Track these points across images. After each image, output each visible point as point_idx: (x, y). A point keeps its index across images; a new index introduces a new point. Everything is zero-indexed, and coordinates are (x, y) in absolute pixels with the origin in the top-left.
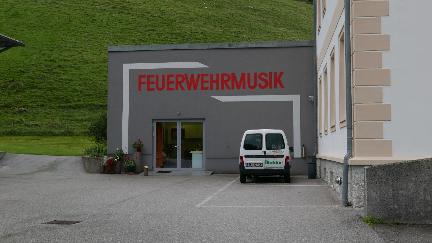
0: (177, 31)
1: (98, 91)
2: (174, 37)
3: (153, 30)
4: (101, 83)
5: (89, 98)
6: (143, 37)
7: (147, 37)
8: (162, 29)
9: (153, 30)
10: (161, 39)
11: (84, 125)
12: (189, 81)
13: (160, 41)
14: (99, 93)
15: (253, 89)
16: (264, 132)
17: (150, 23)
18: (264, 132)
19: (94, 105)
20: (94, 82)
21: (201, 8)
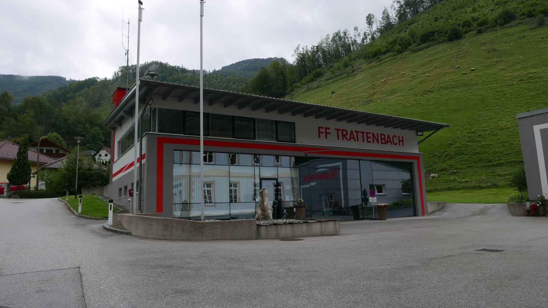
20: (511, 144)
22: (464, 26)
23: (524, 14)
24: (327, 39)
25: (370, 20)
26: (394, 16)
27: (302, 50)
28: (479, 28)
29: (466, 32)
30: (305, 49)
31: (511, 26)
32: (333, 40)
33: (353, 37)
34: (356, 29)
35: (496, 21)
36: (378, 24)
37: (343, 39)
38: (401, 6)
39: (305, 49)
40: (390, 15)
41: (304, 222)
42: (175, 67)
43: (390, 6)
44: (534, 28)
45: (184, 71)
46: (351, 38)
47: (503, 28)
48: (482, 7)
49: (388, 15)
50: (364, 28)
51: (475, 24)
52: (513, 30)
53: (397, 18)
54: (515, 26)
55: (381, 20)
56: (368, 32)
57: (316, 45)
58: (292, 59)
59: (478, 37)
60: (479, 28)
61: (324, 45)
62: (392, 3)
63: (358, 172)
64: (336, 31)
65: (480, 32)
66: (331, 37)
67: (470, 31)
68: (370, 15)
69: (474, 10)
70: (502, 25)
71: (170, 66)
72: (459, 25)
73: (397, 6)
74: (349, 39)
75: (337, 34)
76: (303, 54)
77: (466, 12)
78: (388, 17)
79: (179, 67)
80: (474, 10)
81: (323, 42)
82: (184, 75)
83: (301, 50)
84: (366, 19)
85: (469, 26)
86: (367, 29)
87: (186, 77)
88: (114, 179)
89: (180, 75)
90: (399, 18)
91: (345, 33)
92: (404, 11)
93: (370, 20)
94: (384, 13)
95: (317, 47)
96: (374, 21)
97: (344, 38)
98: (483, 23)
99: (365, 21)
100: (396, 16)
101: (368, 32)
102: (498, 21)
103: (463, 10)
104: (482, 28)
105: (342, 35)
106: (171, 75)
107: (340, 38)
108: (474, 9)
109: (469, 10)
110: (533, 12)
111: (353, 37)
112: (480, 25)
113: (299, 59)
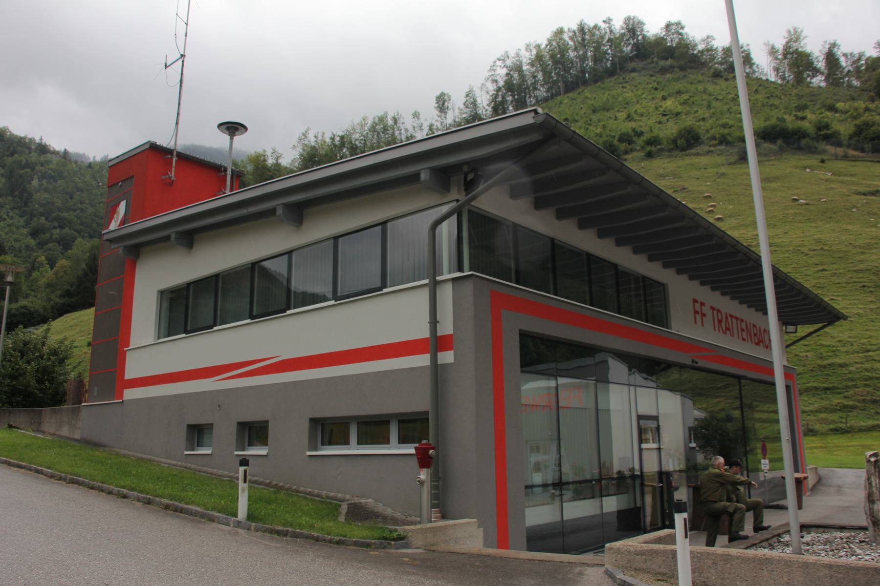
0: (862, 266)
1: (811, 367)
2: (861, 275)
3: (824, 270)
4: (807, 356)
5: (802, 378)
6: (816, 281)
7: (822, 281)
8: (836, 266)
9: (824, 270)
10: (844, 280)
11: (822, 419)
12: (820, 325)
13: (844, 285)
14: (812, 370)
15: (620, 275)
16: (353, 449)
17: (814, 260)
18: (353, 449)
19: (816, 388)
20: (796, 355)
21: (872, 227)
22: (621, 140)
23: (714, 138)
24: (362, 126)
25: (442, 103)
26: (485, 104)
27: (313, 139)
28: (648, 148)
29: (626, 152)
30: (320, 138)
31: (698, 154)
32: (373, 129)
33: (410, 129)
34: (416, 115)
35: (674, 141)
36: (457, 112)
37: (390, 132)
38: (499, 89)
39: (320, 138)
40: (479, 101)
41: (832, 430)
42: (24, 138)
43: (479, 85)
44: (735, 163)
45: (43, 149)
46: (407, 130)
47: (686, 155)
48: (642, 115)
49: (475, 101)
50: (430, 116)
51: (640, 141)
52: (704, 160)
53: (490, 109)
54: (704, 155)
55: (462, 107)
56: (439, 124)
57: (341, 134)
58: (289, 157)
59: (648, 163)
60: (648, 148)
61: (357, 136)
62: (483, 81)
63: (561, 405)
64: (380, 113)
65: (649, 155)
66: (370, 122)
67: (632, 150)
68: (443, 94)
69: (629, 118)
70: (683, 149)
71: (12, 135)
72: (614, 137)
73: (491, 87)
74: (403, 132)
75: (382, 119)
76: (313, 148)
77: (616, 119)
78: (474, 104)
79: (32, 141)
80: (629, 118)
81: (354, 129)
82: (42, 158)
83: (311, 140)
84: (435, 101)
85: (630, 142)
86: (437, 118)
87: (48, 162)
88: (130, 394)
89: (34, 157)
90: (493, 108)
91: (395, 121)
92: (503, 97)
93: (443, 104)
94: (467, 96)
95: (342, 138)
96: (450, 105)
97: (393, 129)
98: (654, 142)
99: (433, 103)
100: (488, 105)
101: (439, 124)
102: (679, 142)
103: (608, 114)
104: (653, 148)
105: (390, 122)
106: (12, 154)
107: (385, 129)
108: (629, 116)
109: (622, 115)
110: (729, 138)
111: (410, 129)
112: (649, 143)
113: (305, 153)
